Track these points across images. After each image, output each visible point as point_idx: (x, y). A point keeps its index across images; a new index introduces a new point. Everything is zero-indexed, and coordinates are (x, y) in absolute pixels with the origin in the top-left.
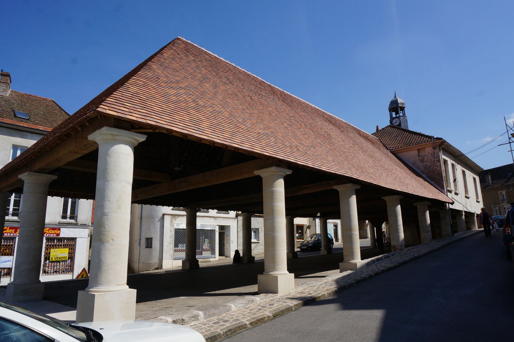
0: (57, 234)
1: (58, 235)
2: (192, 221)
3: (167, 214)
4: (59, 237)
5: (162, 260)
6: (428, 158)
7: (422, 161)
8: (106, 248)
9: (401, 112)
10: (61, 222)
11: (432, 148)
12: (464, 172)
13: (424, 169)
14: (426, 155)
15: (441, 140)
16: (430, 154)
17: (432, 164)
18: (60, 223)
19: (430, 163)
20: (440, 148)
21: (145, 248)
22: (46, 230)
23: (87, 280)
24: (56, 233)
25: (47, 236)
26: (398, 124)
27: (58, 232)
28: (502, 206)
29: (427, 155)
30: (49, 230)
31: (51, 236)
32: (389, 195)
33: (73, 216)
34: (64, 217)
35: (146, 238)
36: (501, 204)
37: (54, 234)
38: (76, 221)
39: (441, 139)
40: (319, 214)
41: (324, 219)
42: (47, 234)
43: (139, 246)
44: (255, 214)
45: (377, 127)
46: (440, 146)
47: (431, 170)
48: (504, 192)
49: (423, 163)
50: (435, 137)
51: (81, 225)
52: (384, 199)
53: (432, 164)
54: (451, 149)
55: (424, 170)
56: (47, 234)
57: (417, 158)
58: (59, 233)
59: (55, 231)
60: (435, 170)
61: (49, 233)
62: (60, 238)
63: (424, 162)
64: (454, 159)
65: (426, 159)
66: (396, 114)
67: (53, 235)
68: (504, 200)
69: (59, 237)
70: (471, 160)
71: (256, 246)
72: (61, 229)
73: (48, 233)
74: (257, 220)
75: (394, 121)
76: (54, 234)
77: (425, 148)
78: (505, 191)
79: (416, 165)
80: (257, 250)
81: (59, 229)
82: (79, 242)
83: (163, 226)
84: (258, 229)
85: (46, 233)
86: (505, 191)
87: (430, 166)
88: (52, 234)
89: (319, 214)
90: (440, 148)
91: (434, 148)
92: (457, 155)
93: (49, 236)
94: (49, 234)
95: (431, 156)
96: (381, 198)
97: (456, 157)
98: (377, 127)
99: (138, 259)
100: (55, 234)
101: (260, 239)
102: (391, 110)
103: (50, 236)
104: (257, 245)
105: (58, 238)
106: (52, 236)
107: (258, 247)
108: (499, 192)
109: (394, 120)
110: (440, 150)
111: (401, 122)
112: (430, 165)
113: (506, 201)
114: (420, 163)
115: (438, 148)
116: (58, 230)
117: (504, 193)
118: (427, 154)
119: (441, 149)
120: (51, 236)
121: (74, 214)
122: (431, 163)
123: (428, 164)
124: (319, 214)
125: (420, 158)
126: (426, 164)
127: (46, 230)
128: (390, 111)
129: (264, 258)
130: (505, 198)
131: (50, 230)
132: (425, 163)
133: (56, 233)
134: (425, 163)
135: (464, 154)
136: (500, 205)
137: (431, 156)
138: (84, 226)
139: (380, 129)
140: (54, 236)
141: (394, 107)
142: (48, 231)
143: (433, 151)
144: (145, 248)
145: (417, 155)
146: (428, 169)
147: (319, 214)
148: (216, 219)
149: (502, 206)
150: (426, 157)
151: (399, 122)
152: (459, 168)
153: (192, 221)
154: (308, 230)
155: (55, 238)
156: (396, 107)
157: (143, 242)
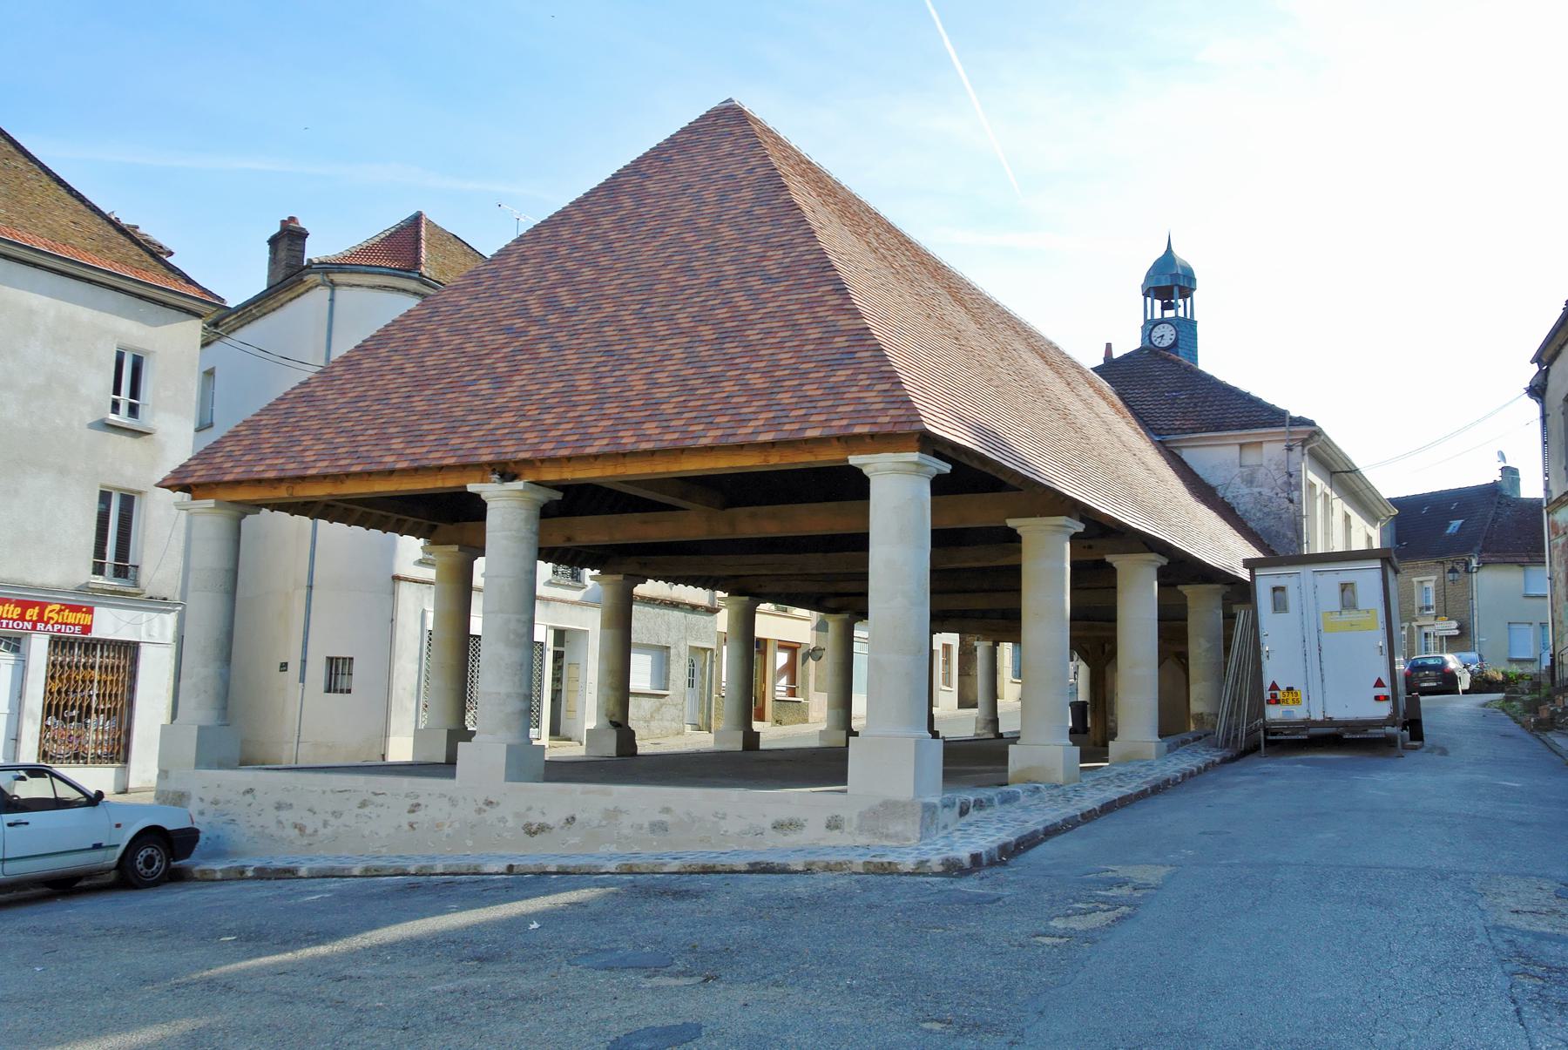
0: (82, 625)
1: (87, 629)
2: (746, 622)
3: (406, 579)
4: (89, 636)
5: (386, 736)
6: (1266, 475)
7: (1250, 481)
10: (93, 586)
11: (1282, 446)
12: (1347, 517)
14: (1261, 465)
15: (1313, 428)
16: (1275, 465)
17: (1277, 494)
18: (84, 589)
19: (1273, 489)
20: (1303, 449)
21: (325, 692)
22: (51, 611)
23: (623, 756)
25: (55, 630)
26: (1171, 342)
27: (86, 619)
28: (1418, 626)
29: (1264, 464)
30: (61, 610)
31: (7, 627)
32: (1200, 583)
34: (99, 569)
35: (327, 657)
36: (1417, 621)
37: (74, 625)
38: (136, 585)
39: (1312, 423)
42: (56, 626)
43: (301, 684)
45: (1109, 346)
46: (1304, 442)
47: (1273, 509)
48: (1431, 580)
49: (1251, 486)
50: (1294, 413)
51: (151, 598)
52: (1181, 592)
54: (1330, 451)
55: (1252, 508)
56: (56, 626)
57: (1237, 470)
58: (89, 623)
59: (79, 615)
60: (1283, 511)
61: (60, 621)
62: (91, 639)
63: (1255, 484)
64: (1329, 479)
65: (1260, 475)
66: (1164, 308)
67: (72, 628)
68: (1428, 608)
69: (89, 636)
70: (1362, 475)
71: (658, 709)
72: (97, 610)
73: (57, 623)
74: (666, 617)
75: (1157, 332)
76: (74, 625)
77: (1261, 442)
78: (1434, 578)
79: (1230, 490)
80: (662, 720)
81: (90, 611)
82: (147, 657)
84: (669, 647)
85: (52, 622)
86: (1434, 578)
87: (1270, 499)
88: (70, 624)
90: (1303, 449)
91: (1289, 449)
92: (1339, 470)
93: (59, 631)
94: (62, 624)
95: (1278, 469)
97: (1335, 472)
98: (1109, 346)
99: (297, 728)
100: (79, 624)
101: (671, 682)
102: (1152, 293)
103: (63, 631)
104: (662, 705)
105: (83, 639)
106: (67, 632)
107: (663, 709)
108: (1415, 580)
109: (1156, 329)
110: (1303, 455)
111: (1180, 337)
112: (1271, 494)
113: (1432, 612)
114: (1242, 486)
115: (1300, 448)
116: (86, 613)
117: (1431, 585)
118: (1265, 463)
119: (1306, 451)
120: (68, 631)
121: (126, 559)
122: (1274, 491)
123: (1266, 491)
125: (1243, 470)
126: (1260, 493)
127: (51, 611)
128: (1146, 295)
129: (1019, 729)
130: (1432, 602)
131: (63, 610)
132: (1258, 490)
133: (81, 623)
134: (1258, 490)
135: (1357, 470)
136: (1414, 624)
137: (1278, 469)
138: (159, 603)
139: (1116, 354)
140: (21, 629)
141: (1164, 285)
142: (58, 613)
143: (1285, 458)
144: (325, 692)
145: (1237, 461)
146: (1265, 506)
148: (548, 605)
149: (1420, 627)
150: (1263, 470)
151: (1173, 337)
152: (1340, 506)
153: (746, 622)
154: (811, 663)
155: (76, 639)
156: (1167, 287)
157: (317, 672)
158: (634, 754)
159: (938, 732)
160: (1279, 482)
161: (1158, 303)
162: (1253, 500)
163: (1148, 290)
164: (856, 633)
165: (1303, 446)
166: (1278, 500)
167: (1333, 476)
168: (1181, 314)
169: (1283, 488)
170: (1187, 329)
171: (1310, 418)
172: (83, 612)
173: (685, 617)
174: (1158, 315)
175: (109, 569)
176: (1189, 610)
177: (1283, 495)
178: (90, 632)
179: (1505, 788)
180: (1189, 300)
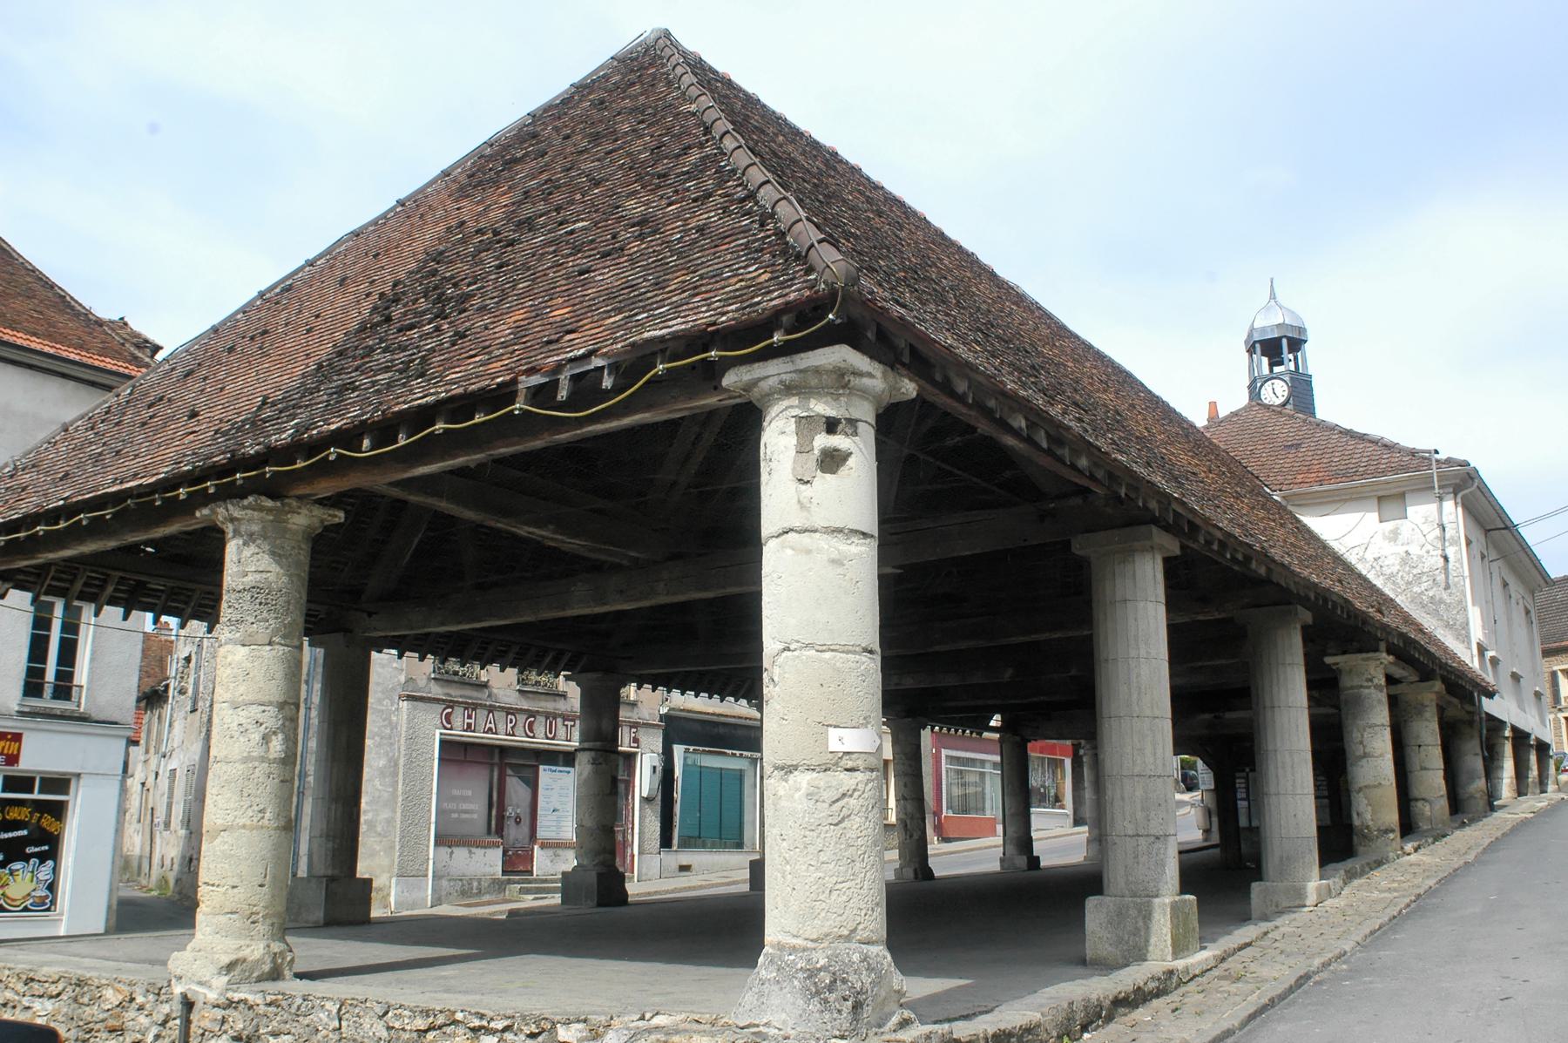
0: (7, 755)
8: (1409, 510)
9: (1291, 356)
13: (1398, 567)
24: (6, 751)
33: (64, 689)
40: (995, 721)
41: (1018, 739)
44: (25, 832)
45: (1213, 405)
53: (1428, 552)
66: (1271, 365)
83: (117, 831)
87: (1420, 557)
89: (995, 721)
96: (1324, 663)
97: (1489, 530)
98: (1213, 405)
116: (11, 740)
119: (1459, 500)
124: (997, 717)
133: (6, 751)
147: (997, 717)
158: (620, 898)
159: (1038, 857)
160: (1430, 537)
161: (1265, 360)
162: (1399, 560)
163: (1253, 346)
164: (1033, 754)
165: (1456, 495)
166: (1429, 558)
167: (1489, 534)
168: (1293, 368)
169: (1435, 544)
170: (1301, 389)
171: (1462, 458)
172: (8, 740)
173: (1442, 796)
174: (1266, 370)
175: (48, 691)
176: (373, 894)
177: (1435, 553)
178: (17, 762)
179: (394, 636)
180: (1299, 354)
